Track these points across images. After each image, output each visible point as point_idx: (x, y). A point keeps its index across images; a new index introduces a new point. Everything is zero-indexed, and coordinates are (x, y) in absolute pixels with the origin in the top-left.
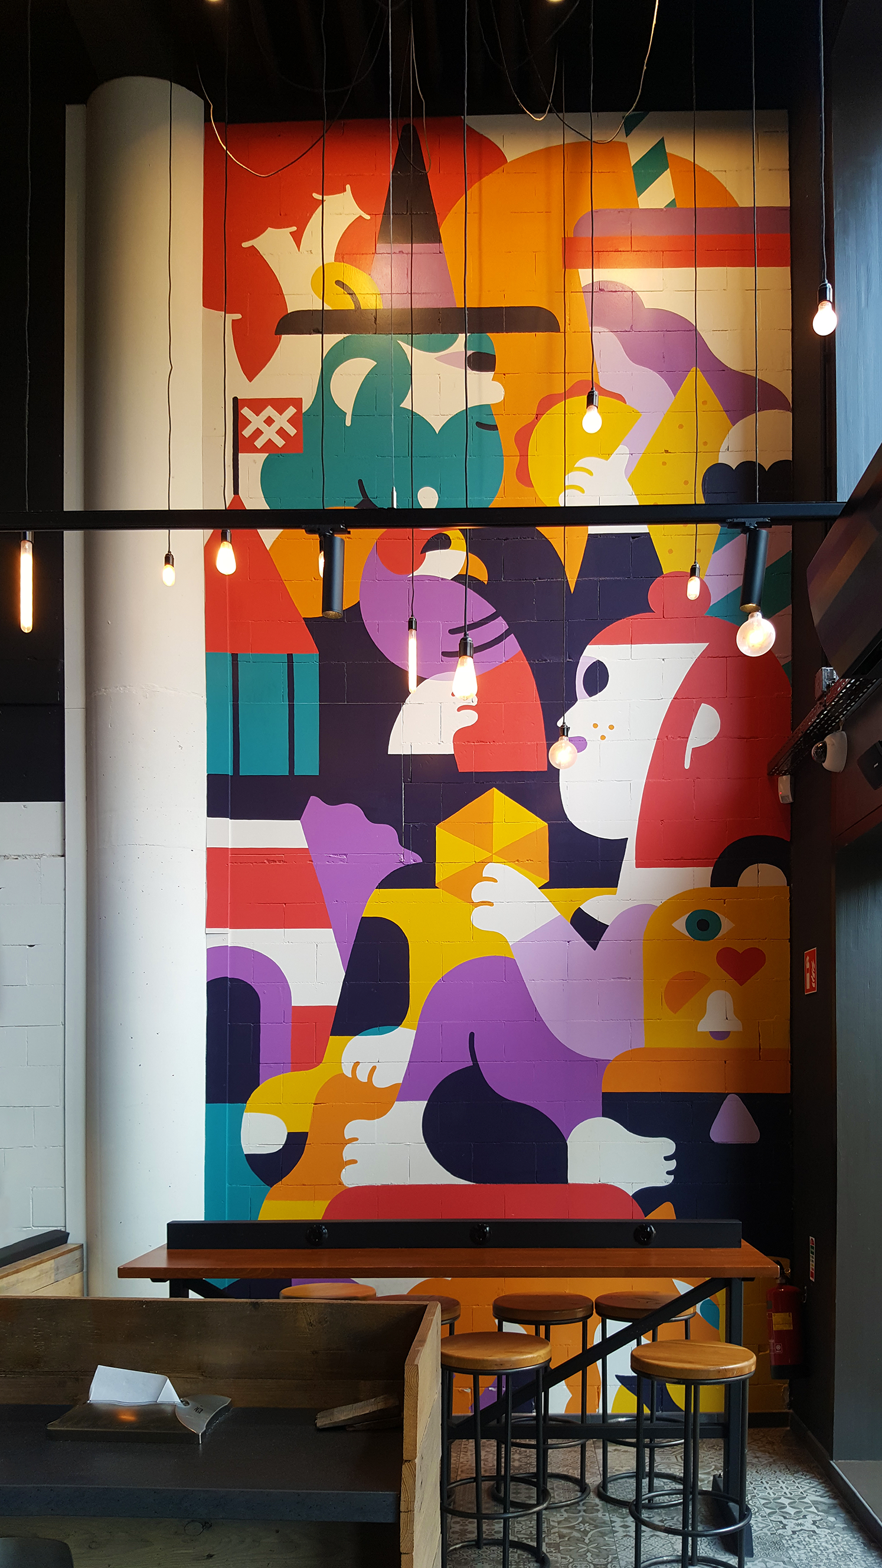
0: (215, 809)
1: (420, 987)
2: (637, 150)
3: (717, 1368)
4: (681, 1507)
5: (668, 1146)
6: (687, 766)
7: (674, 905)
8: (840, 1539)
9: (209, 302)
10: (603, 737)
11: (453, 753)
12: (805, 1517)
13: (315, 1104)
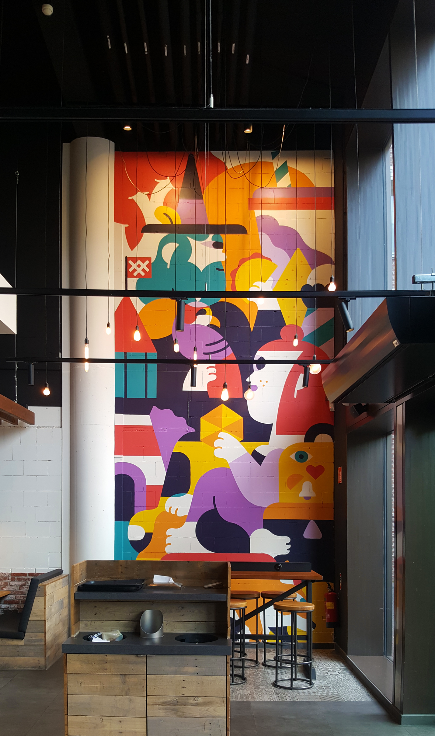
0: (117, 411)
1: (195, 478)
2: (277, 164)
3: (301, 607)
4: (291, 646)
5: (288, 539)
6: (295, 397)
7: (290, 449)
8: (346, 676)
9: (117, 220)
10: (264, 386)
11: (207, 390)
12: (335, 671)
13: (155, 522)
